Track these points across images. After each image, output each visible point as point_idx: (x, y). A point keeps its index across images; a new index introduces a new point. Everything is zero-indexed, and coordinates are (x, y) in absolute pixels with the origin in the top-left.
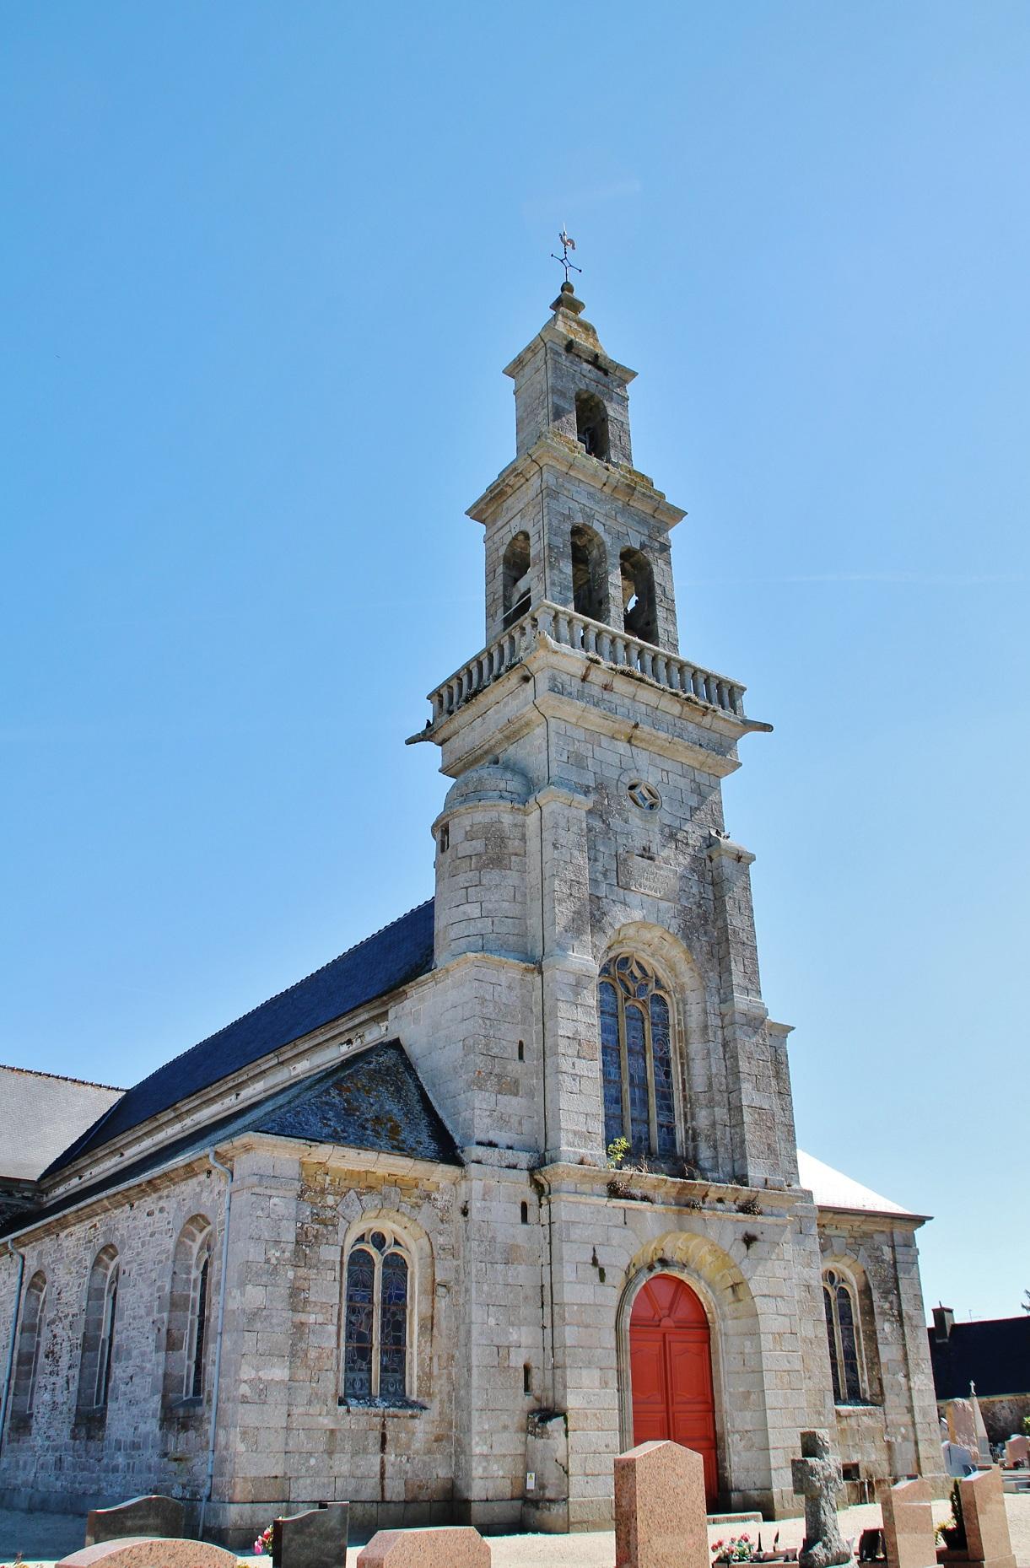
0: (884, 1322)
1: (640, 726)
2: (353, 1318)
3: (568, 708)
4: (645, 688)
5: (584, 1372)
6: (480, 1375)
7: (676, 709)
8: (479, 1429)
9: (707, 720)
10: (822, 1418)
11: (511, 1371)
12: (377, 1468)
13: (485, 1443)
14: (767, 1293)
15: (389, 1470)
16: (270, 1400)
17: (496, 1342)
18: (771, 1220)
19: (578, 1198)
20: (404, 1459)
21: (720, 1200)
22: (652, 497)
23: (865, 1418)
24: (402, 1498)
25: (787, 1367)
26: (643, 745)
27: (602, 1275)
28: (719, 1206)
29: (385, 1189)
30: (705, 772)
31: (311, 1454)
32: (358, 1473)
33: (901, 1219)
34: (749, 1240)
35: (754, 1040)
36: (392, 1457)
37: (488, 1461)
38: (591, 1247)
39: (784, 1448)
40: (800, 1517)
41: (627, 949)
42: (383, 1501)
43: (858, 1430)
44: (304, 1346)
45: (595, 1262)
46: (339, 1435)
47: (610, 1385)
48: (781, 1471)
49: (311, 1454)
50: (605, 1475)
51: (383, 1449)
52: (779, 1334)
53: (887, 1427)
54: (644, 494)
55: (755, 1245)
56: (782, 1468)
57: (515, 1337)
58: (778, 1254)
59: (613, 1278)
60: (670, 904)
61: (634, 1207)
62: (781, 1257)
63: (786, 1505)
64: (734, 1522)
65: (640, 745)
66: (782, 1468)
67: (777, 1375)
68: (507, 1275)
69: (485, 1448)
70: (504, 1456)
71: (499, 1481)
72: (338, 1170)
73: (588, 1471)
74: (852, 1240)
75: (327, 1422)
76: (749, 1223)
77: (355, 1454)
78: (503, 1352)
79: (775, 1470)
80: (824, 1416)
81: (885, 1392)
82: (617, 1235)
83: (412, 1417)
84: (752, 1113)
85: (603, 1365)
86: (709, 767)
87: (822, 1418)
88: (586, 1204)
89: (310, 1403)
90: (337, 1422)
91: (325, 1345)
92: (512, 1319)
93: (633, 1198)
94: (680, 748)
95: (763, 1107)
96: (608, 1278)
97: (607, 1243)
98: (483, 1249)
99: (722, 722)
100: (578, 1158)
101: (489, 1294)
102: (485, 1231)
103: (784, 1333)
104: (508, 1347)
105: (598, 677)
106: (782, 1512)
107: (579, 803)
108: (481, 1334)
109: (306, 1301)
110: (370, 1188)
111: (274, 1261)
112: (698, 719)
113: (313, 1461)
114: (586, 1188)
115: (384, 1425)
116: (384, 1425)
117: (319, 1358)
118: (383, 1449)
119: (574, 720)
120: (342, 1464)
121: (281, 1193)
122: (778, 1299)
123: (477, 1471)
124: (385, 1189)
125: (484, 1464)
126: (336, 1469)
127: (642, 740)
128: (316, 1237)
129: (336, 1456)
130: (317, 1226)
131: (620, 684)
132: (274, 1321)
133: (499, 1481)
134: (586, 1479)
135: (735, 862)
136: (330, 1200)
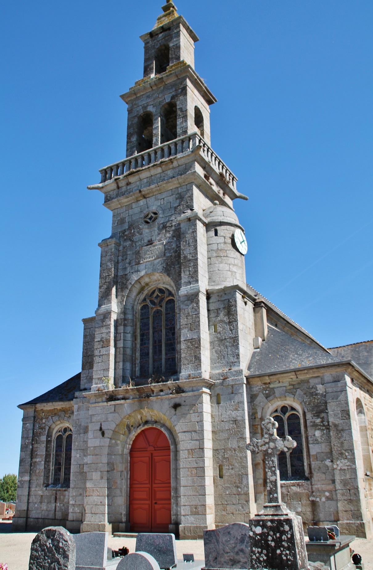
0: (315, 430)
1: (142, 190)
2: (57, 458)
3: (113, 204)
4: (142, 173)
5: (94, 473)
6: (73, 475)
7: (159, 170)
8: (72, 495)
9: (175, 164)
10: (240, 490)
11: (84, 473)
12: (54, 508)
13: (74, 500)
14: (186, 430)
15: (57, 509)
16: (24, 486)
17: (79, 463)
18: (190, 394)
19: (97, 405)
20: (62, 505)
21: (162, 391)
22: (171, 74)
23: (292, 488)
24: (61, 518)
25: (196, 465)
26: (151, 195)
27: (103, 434)
28: (161, 393)
29: (60, 413)
30: (183, 186)
31: (36, 503)
32: (48, 509)
33: (324, 367)
34: (176, 406)
35: (191, 306)
36: (58, 504)
37: (74, 506)
38: (99, 423)
39: (190, 506)
40: (194, 538)
41: (152, 287)
42: (55, 519)
43: (287, 495)
44: (35, 469)
45: (101, 429)
46: (43, 497)
47: (104, 478)
48: (187, 516)
49: (36, 503)
50: (100, 514)
51: (56, 502)
52: (191, 450)
53: (313, 492)
54: (167, 76)
55: (179, 409)
56: (188, 515)
57: (86, 461)
58: (194, 410)
59: (108, 434)
60: (160, 259)
61: (119, 403)
62: (196, 411)
63: (187, 533)
64: (128, 537)
65: (149, 196)
66: (188, 515)
67: (188, 470)
68: (84, 438)
69: (73, 502)
70: (80, 505)
71: (77, 514)
72: (47, 410)
73: (93, 512)
74: (292, 387)
75: (40, 493)
76: (177, 398)
77: (48, 503)
78: (81, 466)
79: (184, 516)
80: (241, 488)
81: (313, 472)
82: (110, 417)
83: (65, 491)
84: (187, 343)
85: (102, 470)
86: (184, 182)
87: (240, 490)
88: (99, 406)
89: (36, 487)
90: (43, 492)
91: (41, 468)
92: (85, 454)
93: (118, 399)
94: (164, 185)
95: (194, 338)
96: (106, 435)
97: (106, 420)
98: (76, 430)
99: (182, 159)
100: (97, 389)
101: (78, 446)
102: (77, 423)
103: (195, 449)
104: (83, 465)
105: (122, 184)
106: (184, 536)
107: (110, 242)
108: (74, 461)
109: (37, 454)
110: (55, 414)
111: (27, 443)
112: (171, 166)
113: (36, 505)
114: (100, 400)
115: (56, 494)
116: (56, 494)
117: (39, 472)
118: (56, 502)
119: (119, 206)
120: (44, 507)
121: (29, 422)
122: (193, 433)
123: (71, 510)
124: (60, 413)
125: (73, 508)
126: (42, 508)
127: (148, 194)
128: (39, 434)
129: (43, 504)
130: (40, 430)
131: (132, 179)
132: (26, 462)
133: (77, 514)
134: (92, 515)
135: (188, 222)
136: (44, 421)
